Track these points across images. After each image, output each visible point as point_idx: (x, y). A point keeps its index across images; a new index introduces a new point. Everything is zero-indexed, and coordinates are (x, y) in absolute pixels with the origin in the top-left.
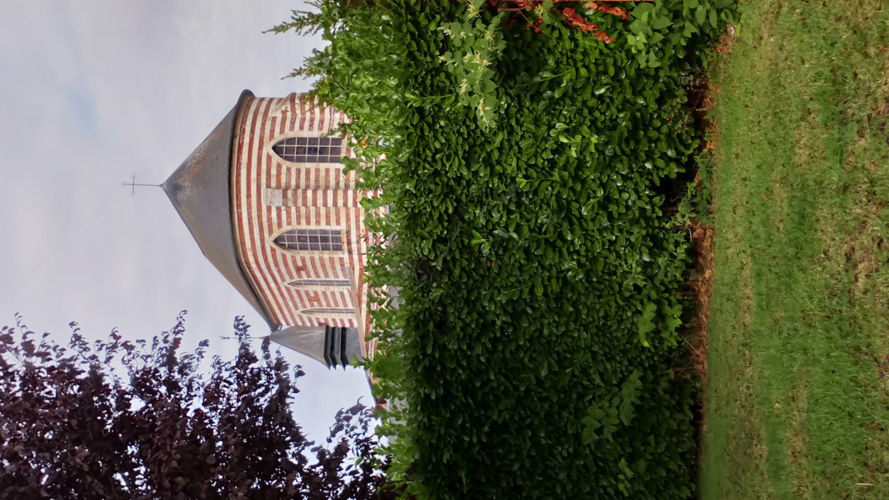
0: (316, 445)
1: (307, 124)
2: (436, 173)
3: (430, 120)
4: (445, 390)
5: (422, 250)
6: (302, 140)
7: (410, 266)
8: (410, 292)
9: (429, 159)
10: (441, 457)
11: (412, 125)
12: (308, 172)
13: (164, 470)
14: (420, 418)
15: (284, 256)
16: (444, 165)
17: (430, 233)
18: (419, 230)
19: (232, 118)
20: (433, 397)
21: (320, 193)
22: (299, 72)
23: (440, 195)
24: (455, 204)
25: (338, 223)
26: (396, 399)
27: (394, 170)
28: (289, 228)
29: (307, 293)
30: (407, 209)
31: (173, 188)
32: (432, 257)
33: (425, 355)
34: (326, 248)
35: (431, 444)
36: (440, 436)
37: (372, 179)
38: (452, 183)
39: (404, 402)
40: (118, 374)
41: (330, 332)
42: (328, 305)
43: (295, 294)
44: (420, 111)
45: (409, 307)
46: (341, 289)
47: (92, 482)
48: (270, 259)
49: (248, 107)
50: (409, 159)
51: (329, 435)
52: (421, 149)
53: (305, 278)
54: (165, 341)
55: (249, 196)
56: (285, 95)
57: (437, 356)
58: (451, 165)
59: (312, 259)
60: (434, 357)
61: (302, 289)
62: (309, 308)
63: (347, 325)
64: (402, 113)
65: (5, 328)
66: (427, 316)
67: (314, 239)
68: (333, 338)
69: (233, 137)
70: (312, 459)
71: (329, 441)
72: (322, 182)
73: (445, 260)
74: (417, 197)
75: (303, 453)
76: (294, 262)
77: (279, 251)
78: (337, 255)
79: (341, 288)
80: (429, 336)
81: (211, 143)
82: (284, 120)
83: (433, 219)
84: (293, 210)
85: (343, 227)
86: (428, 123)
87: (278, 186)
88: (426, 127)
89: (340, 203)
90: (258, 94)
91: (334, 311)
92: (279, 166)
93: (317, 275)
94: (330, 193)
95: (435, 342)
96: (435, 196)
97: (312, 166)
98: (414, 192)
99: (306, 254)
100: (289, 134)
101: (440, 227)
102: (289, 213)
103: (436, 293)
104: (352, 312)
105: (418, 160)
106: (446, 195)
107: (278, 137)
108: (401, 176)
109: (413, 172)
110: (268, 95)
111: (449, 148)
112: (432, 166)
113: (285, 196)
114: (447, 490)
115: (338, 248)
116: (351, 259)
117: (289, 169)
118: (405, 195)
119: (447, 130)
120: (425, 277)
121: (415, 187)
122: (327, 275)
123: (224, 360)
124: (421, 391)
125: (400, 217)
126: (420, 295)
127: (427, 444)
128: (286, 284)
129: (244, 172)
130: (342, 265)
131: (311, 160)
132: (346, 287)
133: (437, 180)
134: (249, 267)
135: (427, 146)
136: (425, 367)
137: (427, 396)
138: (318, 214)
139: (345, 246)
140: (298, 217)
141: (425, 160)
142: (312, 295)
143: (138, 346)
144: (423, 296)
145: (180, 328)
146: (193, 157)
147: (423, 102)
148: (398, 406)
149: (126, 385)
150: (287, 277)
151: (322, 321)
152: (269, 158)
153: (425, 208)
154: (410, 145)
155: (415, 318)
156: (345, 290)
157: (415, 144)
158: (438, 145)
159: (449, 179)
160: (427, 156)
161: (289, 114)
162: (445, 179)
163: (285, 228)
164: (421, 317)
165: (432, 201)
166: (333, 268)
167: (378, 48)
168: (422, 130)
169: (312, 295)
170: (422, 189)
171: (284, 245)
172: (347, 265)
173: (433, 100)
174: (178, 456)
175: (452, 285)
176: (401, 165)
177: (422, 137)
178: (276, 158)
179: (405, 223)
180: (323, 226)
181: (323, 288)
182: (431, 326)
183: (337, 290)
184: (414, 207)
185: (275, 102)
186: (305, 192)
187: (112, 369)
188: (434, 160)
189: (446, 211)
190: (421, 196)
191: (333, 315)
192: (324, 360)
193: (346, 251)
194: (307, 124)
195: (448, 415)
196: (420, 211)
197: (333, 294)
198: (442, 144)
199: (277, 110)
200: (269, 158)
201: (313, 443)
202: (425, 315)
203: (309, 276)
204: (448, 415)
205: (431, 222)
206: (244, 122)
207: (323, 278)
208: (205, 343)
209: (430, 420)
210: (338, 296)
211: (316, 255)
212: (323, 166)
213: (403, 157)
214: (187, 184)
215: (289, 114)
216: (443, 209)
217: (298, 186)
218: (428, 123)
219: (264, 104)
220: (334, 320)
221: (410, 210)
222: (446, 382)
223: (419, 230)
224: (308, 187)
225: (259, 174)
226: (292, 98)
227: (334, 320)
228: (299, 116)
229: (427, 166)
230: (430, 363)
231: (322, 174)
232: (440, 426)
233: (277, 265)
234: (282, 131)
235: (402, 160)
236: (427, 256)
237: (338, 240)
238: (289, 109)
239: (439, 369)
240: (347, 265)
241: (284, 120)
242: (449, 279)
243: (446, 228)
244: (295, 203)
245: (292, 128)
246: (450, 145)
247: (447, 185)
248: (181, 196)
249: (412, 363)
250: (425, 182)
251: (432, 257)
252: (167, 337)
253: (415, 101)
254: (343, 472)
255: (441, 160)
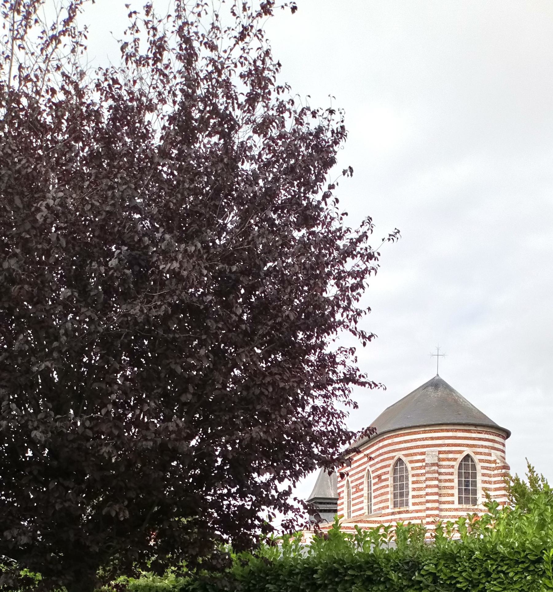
0: (293, 489)
1: (487, 479)
2: (488, 574)
3: (531, 568)
4: (320, 585)
5: (428, 565)
6: (474, 476)
7: (415, 556)
8: (394, 557)
9: (499, 569)
10: (270, 583)
11: (527, 554)
12: (451, 481)
13: (278, 377)
14: (298, 567)
15: (388, 466)
16: (495, 579)
17: (441, 571)
18: (443, 562)
19: (490, 424)
20: (315, 576)
21: (436, 490)
22: (531, 470)
23: (471, 577)
24: (464, 589)
25: (414, 504)
26: (309, 549)
27: (490, 542)
28: (409, 469)
29: (362, 483)
30: (459, 552)
31: (436, 384)
32: (422, 572)
33: (347, 569)
34: (395, 496)
35: (279, 575)
36: (285, 581)
37: (483, 525)
38: (481, 586)
39: (307, 555)
40: (335, 342)
41: (333, 501)
42: (353, 499)
43: (360, 475)
44: (540, 560)
45: (382, 556)
46: (366, 508)
47: (268, 325)
48: (386, 456)
49: (499, 436)
50: (500, 553)
51: (300, 499)
52: (508, 562)
53: (373, 481)
54: (360, 376)
55: (432, 439)
56: (508, 461)
57: (346, 578)
58: (495, 585)
59: (387, 486)
60: (345, 576)
61: (364, 480)
62: (351, 485)
63: (339, 513)
64: (536, 547)
65: (379, 254)
66: (376, 570)
67: (402, 488)
68: (328, 503)
69: (476, 425)
70: (282, 486)
71: (295, 499)
72: (444, 491)
73: (421, 582)
74: (469, 560)
75: (286, 480)
76: (385, 473)
77: (392, 462)
78: (390, 504)
79: (367, 508)
80: (361, 571)
81: (469, 410)
82: (489, 462)
83: (451, 572)
84: (423, 471)
85: (411, 508)
86: (529, 567)
87: (439, 460)
88: (526, 565)
89: (429, 505)
90: (507, 442)
91: (349, 503)
92: (455, 459)
93: (375, 490)
94: (436, 497)
95: (356, 576)
96: (470, 574)
97: (456, 484)
98: (473, 558)
99: (390, 482)
100: (479, 466)
101: (446, 578)
102: (420, 468)
103: (393, 576)
104: (349, 516)
105: (499, 560)
106: (471, 582)
107: (476, 458)
108: (485, 547)
109: (488, 556)
110: (506, 449)
111: (509, 583)
112: (494, 570)
113: (433, 465)
114: (246, 588)
115: (395, 505)
116: (388, 515)
117: (453, 467)
118: (470, 551)
119: (523, 581)
120: (406, 567)
121: (477, 558)
122: (375, 497)
123: (345, 420)
124: (319, 567)
125: (453, 548)
126: (392, 564)
127: (280, 572)
128: (369, 468)
129: (450, 434)
130: (383, 508)
131: (460, 483)
132: (367, 511)
133: (483, 575)
134: (380, 441)
135: (510, 566)
136: (337, 569)
137: (316, 572)
138: (420, 489)
139: (397, 510)
140: (418, 475)
141: (498, 565)
142: (361, 487)
143: (352, 358)
144: (391, 566)
145: (373, 385)
146: (460, 397)
147: (547, 563)
148: (303, 551)
149: (327, 350)
150: (373, 468)
151: (341, 495)
152: (460, 452)
153: (460, 566)
154: (509, 553)
155: (374, 561)
156: (365, 510)
157: (511, 557)
158: (511, 575)
159: (484, 584)
160: (502, 566)
161: (493, 465)
162: (484, 581)
163: (409, 466)
164: (375, 566)
165: (466, 571)
166: (381, 502)
167: (410, 537)
168: (523, 562)
169: (361, 487)
170: (476, 564)
171: (397, 466)
172: (384, 512)
173: (549, 570)
174: (287, 387)
175: (400, 588)
176: (495, 547)
177: (517, 562)
178: (460, 457)
179: (448, 552)
180: (411, 493)
181: (366, 495)
182: (369, 573)
183: (365, 505)
184: (461, 558)
185: (502, 454)
186: (437, 479)
187: (334, 340)
188: (499, 572)
189: (458, 582)
190: (470, 563)
191: (346, 503)
192: (312, 497)
193: (393, 511)
194: (487, 479)
195: (301, 587)
196: (457, 563)
197: (362, 502)
198: (512, 578)
199: (497, 456)
200: (460, 452)
201: (295, 487)
202: (377, 568)
203: (374, 484)
204: (301, 587)
205: (448, 571)
206: (487, 433)
207: (373, 495)
208: (356, 406)
209: (297, 574)
210: (360, 506)
211: (390, 489)
212: (456, 492)
213: (501, 548)
214: (440, 393)
215: (493, 465)
216: (460, 579)
217: (440, 474)
218: (529, 567)
219: (501, 447)
220: (342, 503)
221: (458, 554)
222: (326, 585)
223: (443, 562)
224: (440, 481)
225: (448, 445)
226: (506, 467)
227: (342, 503)
228: (492, 473)
229: (494, 567)
230: (341, 573)
231: (450, 491)
232: (294, 582)
233: (382, 461)
234: (481, 461)
235: (498, 548)
236: (422, 568)
237: (402, 504)
238: (497, 465)
239: (336, 580)
240: (384, 512)
241: (489, 462)
242: (405, 586)
243: (445, 583)
244: (428, 472)
245: (483, 468)
246: (511, 584)
247: (480, 583)
248: (430, 389)
249: (341, 560)
250: (481, 566)
251: (422, 572)
252: (363, 377)
253: (548, 556)
254: (272, 511)
255: (499, 578)
